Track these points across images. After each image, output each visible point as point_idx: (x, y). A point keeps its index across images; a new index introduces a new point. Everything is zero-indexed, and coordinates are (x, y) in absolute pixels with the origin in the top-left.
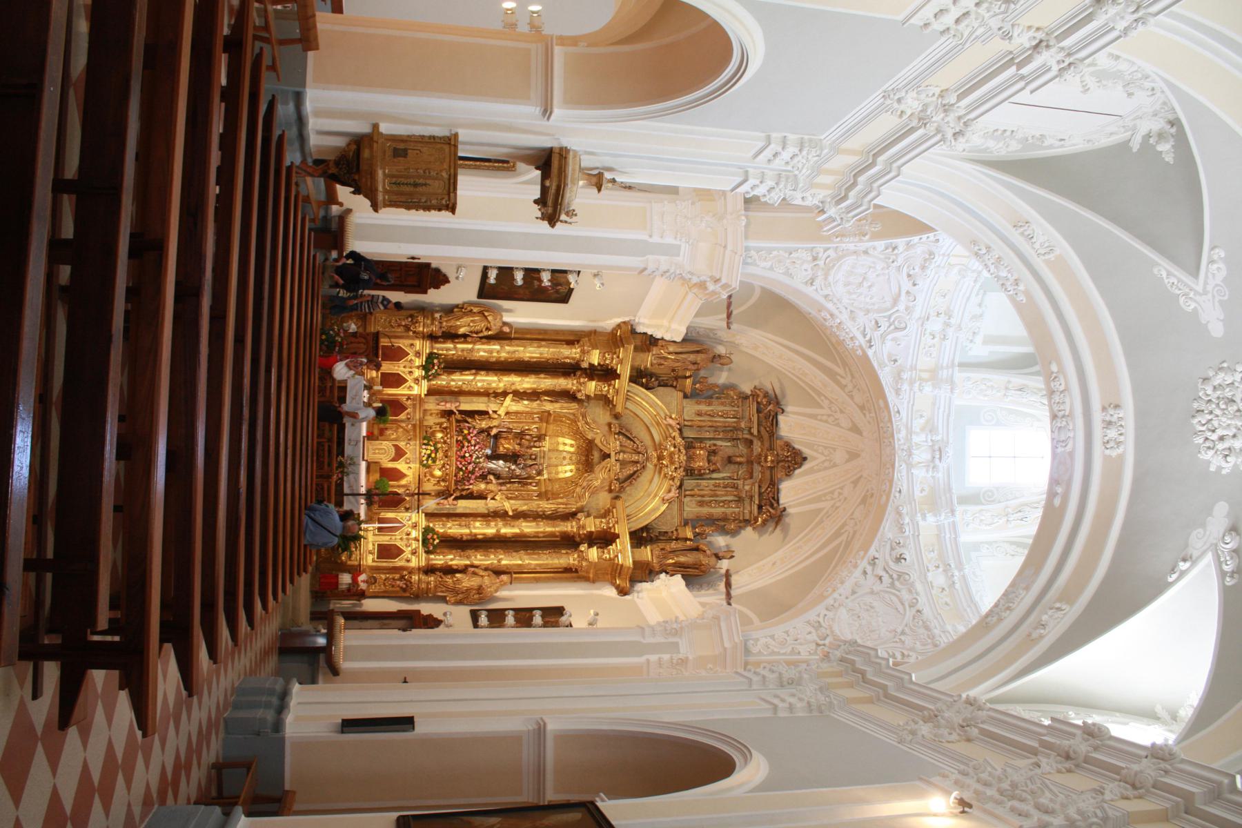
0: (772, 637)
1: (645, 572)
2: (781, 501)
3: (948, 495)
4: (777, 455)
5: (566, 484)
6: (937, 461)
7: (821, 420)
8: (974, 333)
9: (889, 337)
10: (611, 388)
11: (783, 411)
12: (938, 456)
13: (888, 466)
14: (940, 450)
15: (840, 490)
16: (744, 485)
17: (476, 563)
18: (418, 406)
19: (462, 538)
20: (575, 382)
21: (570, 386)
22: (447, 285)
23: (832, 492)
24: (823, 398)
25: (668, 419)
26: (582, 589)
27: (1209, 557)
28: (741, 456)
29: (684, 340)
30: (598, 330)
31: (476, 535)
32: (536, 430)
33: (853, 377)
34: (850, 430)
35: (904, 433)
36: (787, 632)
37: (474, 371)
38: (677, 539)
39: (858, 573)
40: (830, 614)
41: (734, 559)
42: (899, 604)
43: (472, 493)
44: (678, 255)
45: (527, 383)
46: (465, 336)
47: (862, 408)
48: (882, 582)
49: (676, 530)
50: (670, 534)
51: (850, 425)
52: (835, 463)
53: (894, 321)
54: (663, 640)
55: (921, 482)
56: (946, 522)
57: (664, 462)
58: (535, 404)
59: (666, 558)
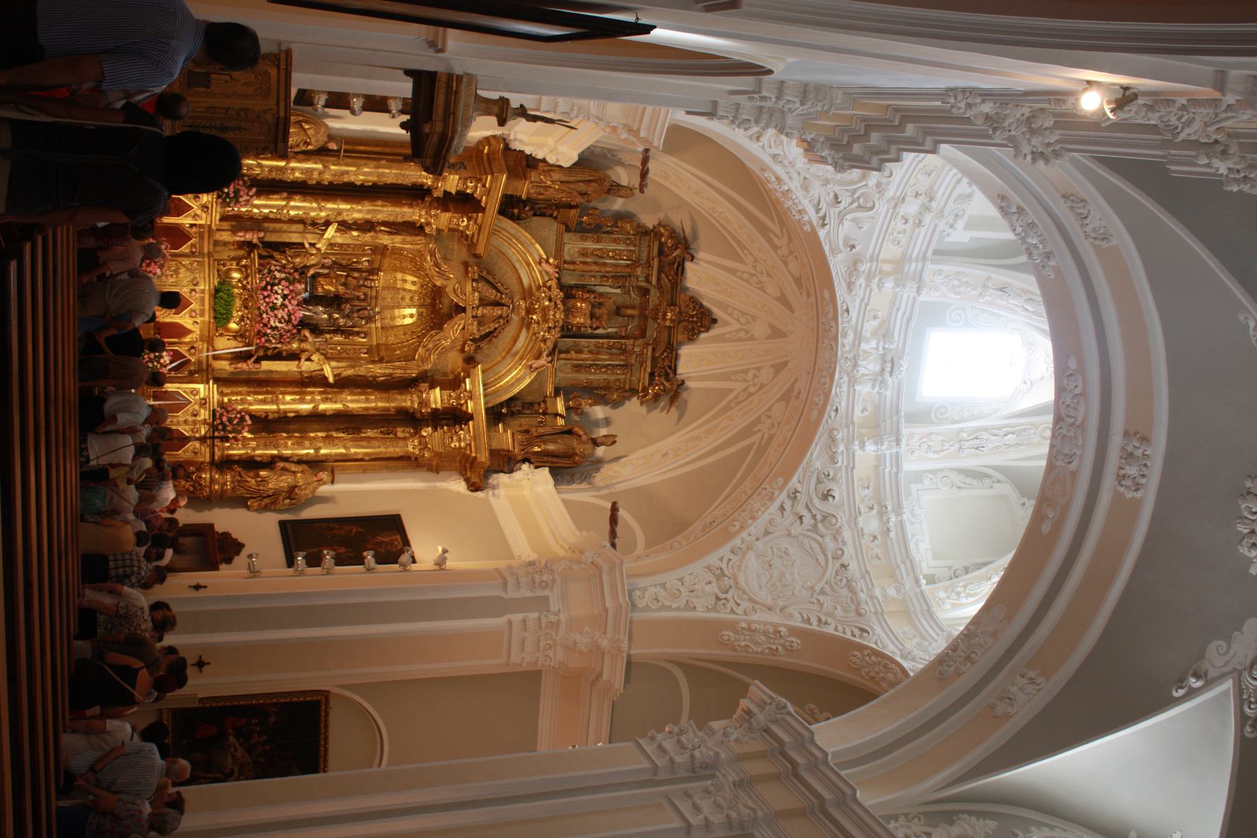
0: (663, 586)
1: (505, 462)
2: (679, 371)
3: (895, 418)
5: (405, 334)
6: (887, 375)
7: (741, 278)
8: (957, 216)
9: (849, 217)
10: (471, 223)
11: (693, 258)
12: (888, 369)
13: (824, 374)
14: (892, 362)
15: (755, 371)
16: (633, 345)
17: (287, 452)
20: (423, 213)
23: (746, 371)
25: (543, 265)
26: (423, 481)
27: (1228, 685)
28: (633, 308)
31: (286, 412)
32: (366, 264)
33: (790, 240)
34: (777, 299)
35: (851, 336)
36: (681, 580)
37: (285, 195)
40: (735, 558)
41: (616, 444)
42: (819, 551)
45: (356, 211)
47: (798, 281)
48: (802, 523)
51: (779, 294)
52: (752, 335)
53: (858, 198)
54: (529, 594)
55: (863, 399)
56: (888, 453)
57: (534, 317)
59: (530, 443)
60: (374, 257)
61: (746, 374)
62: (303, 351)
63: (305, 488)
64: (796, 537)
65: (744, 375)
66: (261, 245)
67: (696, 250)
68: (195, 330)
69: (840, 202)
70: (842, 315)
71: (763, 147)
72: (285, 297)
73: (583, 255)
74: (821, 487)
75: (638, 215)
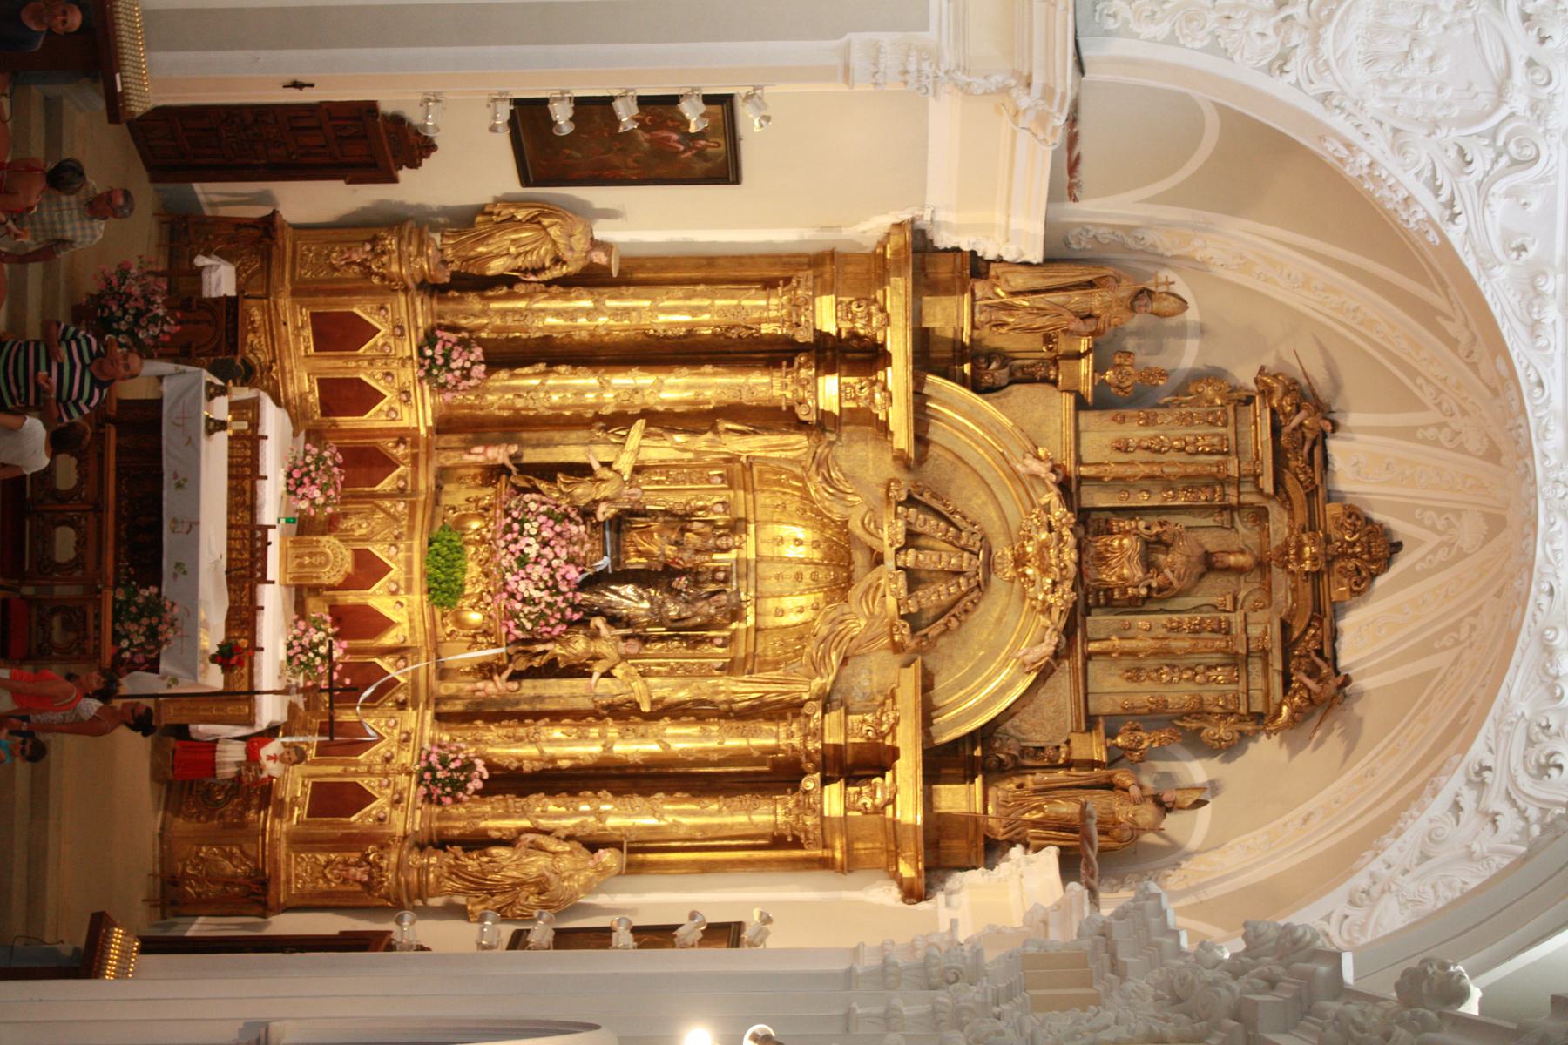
4: (1328, 540)
7: (1425, 441)
9: (1500, 187)
11: (1335, 426)
15: (1471, 620)
17: (544, 823)
18: (422, 458)
19: (520, 769)
21: (776, 392)
22: (433, 155)
23: (1456, 627)
24: (1420, 381)
29: (1049, 260)
30: (840, 249)
31: (553, 759)
32: (720, 508)
37: (541, 367)
38: (1068, 765)
39: (1438, 807)
40: (1356, 914)
43: (553, 662)
44: (926, 29)
46: (507, 281)
48: (1496, 829)
49: (1068, 742)
50: (1050, 752)
52: (1460, 549)
53: (1505, 144)
58: (702, 442)
60: (731, 493)
61: (1458, 631)
62: (596, 658)
63: (571, 876)
64: (1484, 858)
65: (1455, 635)
66: (514, 469)
67: (1341, 411)
68: (395, 618)
69: (1470, 163)
70: (1530, 394)
71: (1298, 84)
72: (545, 544)
73: (1118, 449)
74: (1533, 754)
75: (1231, 371)
